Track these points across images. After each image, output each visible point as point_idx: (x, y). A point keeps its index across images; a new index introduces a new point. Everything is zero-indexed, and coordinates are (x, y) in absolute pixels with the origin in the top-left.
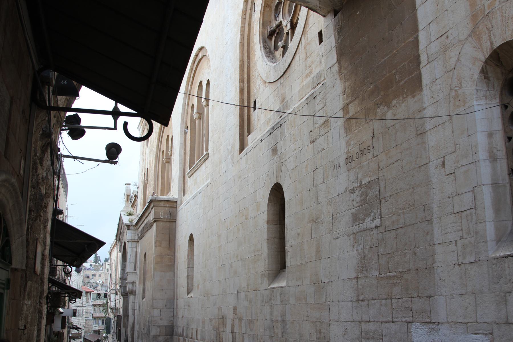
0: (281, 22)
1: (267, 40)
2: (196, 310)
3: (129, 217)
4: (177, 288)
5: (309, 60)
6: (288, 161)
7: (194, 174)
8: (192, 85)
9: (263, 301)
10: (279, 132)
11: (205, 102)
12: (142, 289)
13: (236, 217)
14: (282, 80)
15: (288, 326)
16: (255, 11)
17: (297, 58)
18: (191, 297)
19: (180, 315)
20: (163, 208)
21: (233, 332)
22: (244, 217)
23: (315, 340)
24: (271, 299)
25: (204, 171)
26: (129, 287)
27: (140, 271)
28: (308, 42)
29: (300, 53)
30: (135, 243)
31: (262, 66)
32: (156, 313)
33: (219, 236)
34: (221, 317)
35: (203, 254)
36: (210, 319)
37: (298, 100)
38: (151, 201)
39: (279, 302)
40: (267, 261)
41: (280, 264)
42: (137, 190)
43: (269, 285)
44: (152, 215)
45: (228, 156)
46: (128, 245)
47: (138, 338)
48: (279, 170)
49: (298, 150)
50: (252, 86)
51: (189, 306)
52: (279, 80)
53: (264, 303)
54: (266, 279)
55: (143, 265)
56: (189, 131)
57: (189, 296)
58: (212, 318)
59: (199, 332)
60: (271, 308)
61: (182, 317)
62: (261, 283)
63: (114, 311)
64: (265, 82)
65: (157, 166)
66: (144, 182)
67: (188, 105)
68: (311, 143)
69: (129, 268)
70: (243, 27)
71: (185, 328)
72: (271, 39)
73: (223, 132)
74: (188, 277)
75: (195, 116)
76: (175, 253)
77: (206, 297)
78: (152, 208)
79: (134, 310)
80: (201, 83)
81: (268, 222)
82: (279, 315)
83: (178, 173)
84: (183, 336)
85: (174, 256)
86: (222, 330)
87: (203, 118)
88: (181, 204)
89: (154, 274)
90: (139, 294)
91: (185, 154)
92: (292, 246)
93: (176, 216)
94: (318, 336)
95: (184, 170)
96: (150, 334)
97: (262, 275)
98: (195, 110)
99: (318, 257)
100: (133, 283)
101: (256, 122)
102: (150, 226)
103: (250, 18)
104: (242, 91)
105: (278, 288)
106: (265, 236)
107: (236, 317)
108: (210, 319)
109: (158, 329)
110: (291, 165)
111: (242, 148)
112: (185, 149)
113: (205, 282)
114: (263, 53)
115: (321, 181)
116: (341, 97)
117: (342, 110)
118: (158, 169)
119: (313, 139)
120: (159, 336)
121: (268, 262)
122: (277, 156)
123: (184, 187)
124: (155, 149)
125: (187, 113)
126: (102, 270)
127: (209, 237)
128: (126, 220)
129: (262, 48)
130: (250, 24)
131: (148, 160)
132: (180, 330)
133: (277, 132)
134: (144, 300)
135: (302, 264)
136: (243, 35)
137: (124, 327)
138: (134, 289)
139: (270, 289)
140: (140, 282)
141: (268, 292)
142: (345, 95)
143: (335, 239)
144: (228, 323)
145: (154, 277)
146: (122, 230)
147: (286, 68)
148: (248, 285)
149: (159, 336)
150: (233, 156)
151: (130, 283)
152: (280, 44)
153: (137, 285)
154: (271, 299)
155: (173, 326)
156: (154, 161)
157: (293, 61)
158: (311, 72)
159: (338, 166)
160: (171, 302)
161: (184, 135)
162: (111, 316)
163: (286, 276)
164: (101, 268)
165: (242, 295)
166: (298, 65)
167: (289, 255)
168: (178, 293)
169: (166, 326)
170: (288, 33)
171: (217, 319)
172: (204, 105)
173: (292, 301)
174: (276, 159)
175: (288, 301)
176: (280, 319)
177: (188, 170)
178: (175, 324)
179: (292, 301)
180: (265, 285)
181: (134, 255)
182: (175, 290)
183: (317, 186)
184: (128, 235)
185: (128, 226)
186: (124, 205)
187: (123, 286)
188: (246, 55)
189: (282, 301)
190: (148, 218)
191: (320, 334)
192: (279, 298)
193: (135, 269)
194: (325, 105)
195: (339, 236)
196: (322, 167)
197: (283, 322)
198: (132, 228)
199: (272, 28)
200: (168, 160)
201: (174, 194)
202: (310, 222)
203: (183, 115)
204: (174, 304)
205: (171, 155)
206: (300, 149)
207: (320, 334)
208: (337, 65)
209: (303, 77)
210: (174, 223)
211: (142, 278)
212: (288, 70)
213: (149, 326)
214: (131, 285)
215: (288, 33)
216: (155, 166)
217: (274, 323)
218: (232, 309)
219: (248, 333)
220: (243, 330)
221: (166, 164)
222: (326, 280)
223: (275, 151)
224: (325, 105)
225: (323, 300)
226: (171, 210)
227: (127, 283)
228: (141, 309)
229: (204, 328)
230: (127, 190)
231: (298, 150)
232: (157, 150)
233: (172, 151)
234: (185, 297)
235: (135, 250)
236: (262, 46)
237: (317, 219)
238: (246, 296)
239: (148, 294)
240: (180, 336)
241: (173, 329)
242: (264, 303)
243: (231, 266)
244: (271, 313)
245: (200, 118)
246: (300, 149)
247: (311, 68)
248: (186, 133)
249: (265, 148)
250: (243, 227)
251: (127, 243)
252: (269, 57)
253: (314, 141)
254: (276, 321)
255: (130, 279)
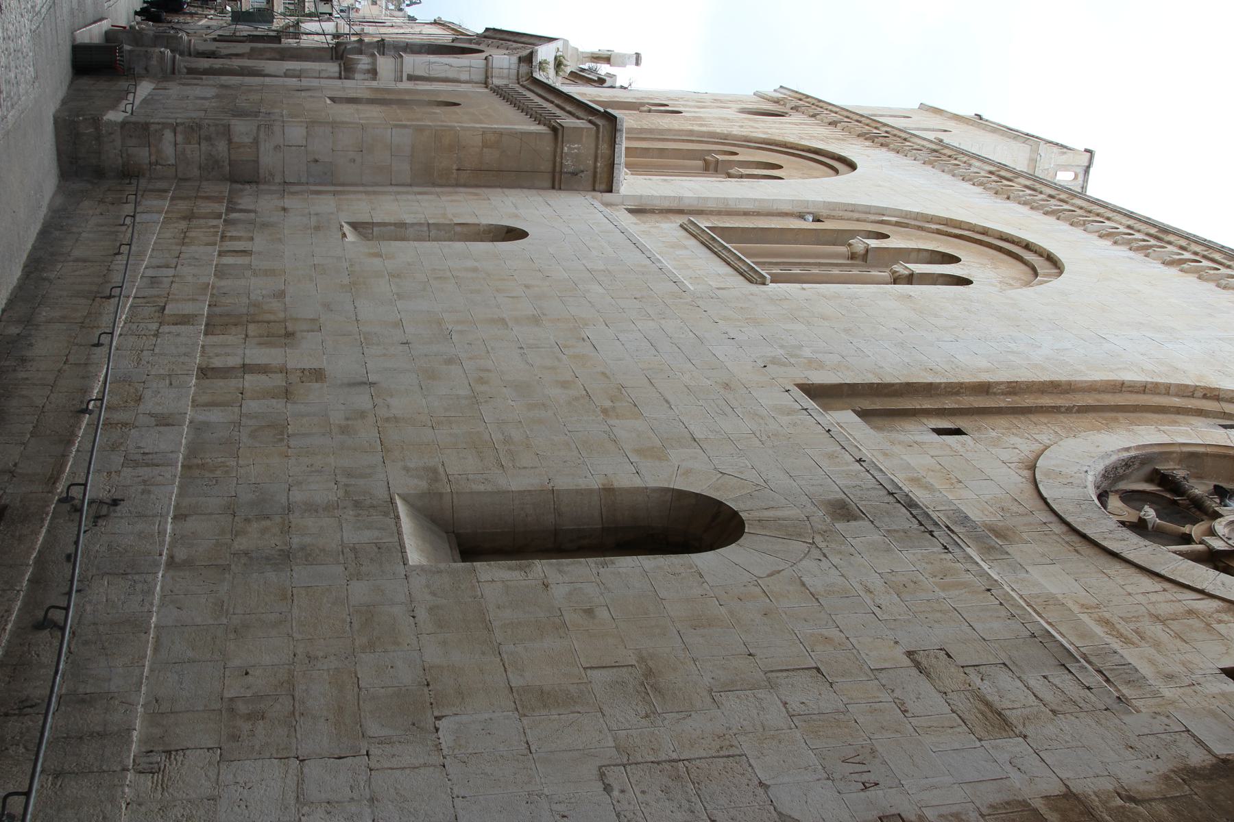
0: (1220, 516)
1: (1147, 469)
2: (306, 252)
3: (551, 60)
4: (366, 193)
5: (1157, 630)
6: (825, 564)
7: (693, 242)
8: (939, 232)
9: (349, 475)
10: (907, 526)
11: (906, 272)
12: (359, 95)
13: (603, 374)
14: (1058, 528)
15: (271, 576)
16: (1225, 427)
17: (1147, 583)
18: (344, 235)
19: (288, 202)
20: (592, 151)
21: (246, 368)
22: (608, 404)
23: (227, 695)
24: (357, 505)
25: (706, 270)
26: (363, 62)
27: (407, 91)
28: (1215, 626)
29: (1168, 596)
30: (481, 77)
31: (1082, 455)
32: (296, 133)
33: (536, 320)
34: (290, 329)
35: (475, 270)
36: (281, 295)
37: (1024, 593)
38: (612, 119)
39: (352, 536)
40: (482, 488)
41: (482, 538)
42: (618, 85)
43: (405, 499)
44: (569, 122)
45: (782, 347)
46: (476, 61)
47: (223, 86)
48: (790, 530)
49: (869, 601)
50: (1002, 422)
51: (317, 228)
52: (1053, 518)
53: (343, 480)
54: (424, 485)
55: (426, 98)
56: (809, 224)
57: (347, 229)
58: (287, 299)
59: (240, 260)
60: (329, 508)
61: (284, 209)
62: (407, 469)
63: (291, 30)
64: (1033, 468)
65: (690, 137)
66: (643, 104)
67: (882, 222)
68: (910, 654)
69: (413, 63)
70: (1167, 390)
71: (252, 215)
72: (1149, 480)
73: (847, 331)
74: (402, 225)
75: (859, 244)
76: (465, 186)
77: (346, 281)
78: (590, 121)
79: (299, 75)
80: (954, 260)
81: (608, 491)
82: (308, 540)
83: (691, 195)
84: (230, 210)
85: (458, 185)
86: (250, 333)
87: (852, 265)
88: (607, 205)
89: (405, 126)
90: (344, 89)
91: (746, 214)
92: (546, 586)
93: (571, 188)
94: (242, 708)
95: (700, 212)
96: (234, 116)
97: (435, 471)
98: (873, 243)
99: (532, 700)
100: (373, 73)
101: (901, 437)
102: (538, 118)
103: (1200, 413)
104: (984, 389)
105: (400, 533)
106: (564, 482)
107: (294, 378)
108: (281, 295)
109: (247, 140)
110: (817, 574)
111: (816, 392)
112: (758, 214)
113: (391, 275)
114: (1114, 458)
115: (794, 705)
116: (1108, 785)
117: (1064, 789)
118: (683, 141)
119: (924, 662)
120: (230, 141)
121: (479, 493)
122: (828, 520)
123: (652, 211)
124: (736, 131)
125: (858, 220)
126: (387, 8)
127: (527, 287)
128: (545, 53)
129: (1126, 455)
130: (1180, 411)
131: (703, 113)
132: (245, 202)
133: (903, 520)
134: (328, 101)
135: (489, 628)
136: (1144, 392)
137: (252, 49)
138: (357, 76)
139: (392, 501)
140: (377, 90)
141: (381, 494)
142: (1119, 802)
143: (602, 776)
144: (273, 351)
145: (396, 126)
146: (515, 45)
147: (1105, 544)
148: (396, 419)
149: (230, 141)
150: (784, 365)
151: (374, 63)
152: (1150, 513)
153: (367, 83)
154: (357, 505)
155: (257, 183)
156: (704, 129)
157: (1132, 570)
158: (1127, 641)
159: (865, 777)
160: (325, 177)
161: (797, 210)
162: (278, 23)
163: (442, 566)
164: (391, 7)
165: (362, 400)
166: (1129, 589)
167: (516, 575)
168: (352, 196)
169: (257, 162)
170: (1187, 539)
171: (281, 315)
172: (896, 268)
173: (360, 591)
174: (820, 517)
175: (359, 576)
176: (296, 541)
177: (704, 223)
178: (262, 187)
179: (360, 591)
180: (404, 483)
181: (451, 75)
182: (361, 189)
183: (772, 686)
184: (504, 61)
185: (529, 59)
186: (581, 50)
187: (361, 47)
188: (1090, 400)
189: (353, 549)
190: (558, 112)
191: (249, 717)
192: (367, 536)
193: (411, 78)
194: (1053, 711)
195: (616, 793)
196: (841, 707)
197: (285, 557)
198: (524, 68)
199: (1186, 485)
200: (712, 166)
201: (631, 184)
202: (642, 659)
203: (853, 208)
204: (320, 184)
205: (730, 176)
206: (877, 610)
207: (249, 717)
208: (1209, 760)
209: (1098, 606)
210: (549, 184)
211: (387, 96)
212: (1096, 550)
213: (257, 114)
214: (367, 67)
215: (1187, 539)
216: (691, 132)
217: (278, 519)
218: (315, 365)
219: (244, 420)
220: (252, 406)
221: (701, 163)
222: (446, 738)
223: (843, 511)
224: (1053, 711)
225: (374, 729)
226: (586, 176)
227: (373, 55)
228: (303, 94)
229: (255, 274)
230: (624, 56)
231: (869, 601)
232: (736, 138)
233: (741, 177)
234: (344, 218)
235: (464, 77)
236: (1133, 453)
237: (655, 688)
238: (362, 415)
239: (346, 112)
240: (230, 201)
241: (249, 182)
242: (343, 480)
243: (450, 361)
244: (311, 508)
245: (853, 256)
246: (877, 610)
247: (1135, 638)
248: (801, 216)
249: (841, 478)
250: (577, 399)
251: (483, 55)
252: (1104, 476)
253: (917, 665)
254: (286, 529)
255: (385, 64)
